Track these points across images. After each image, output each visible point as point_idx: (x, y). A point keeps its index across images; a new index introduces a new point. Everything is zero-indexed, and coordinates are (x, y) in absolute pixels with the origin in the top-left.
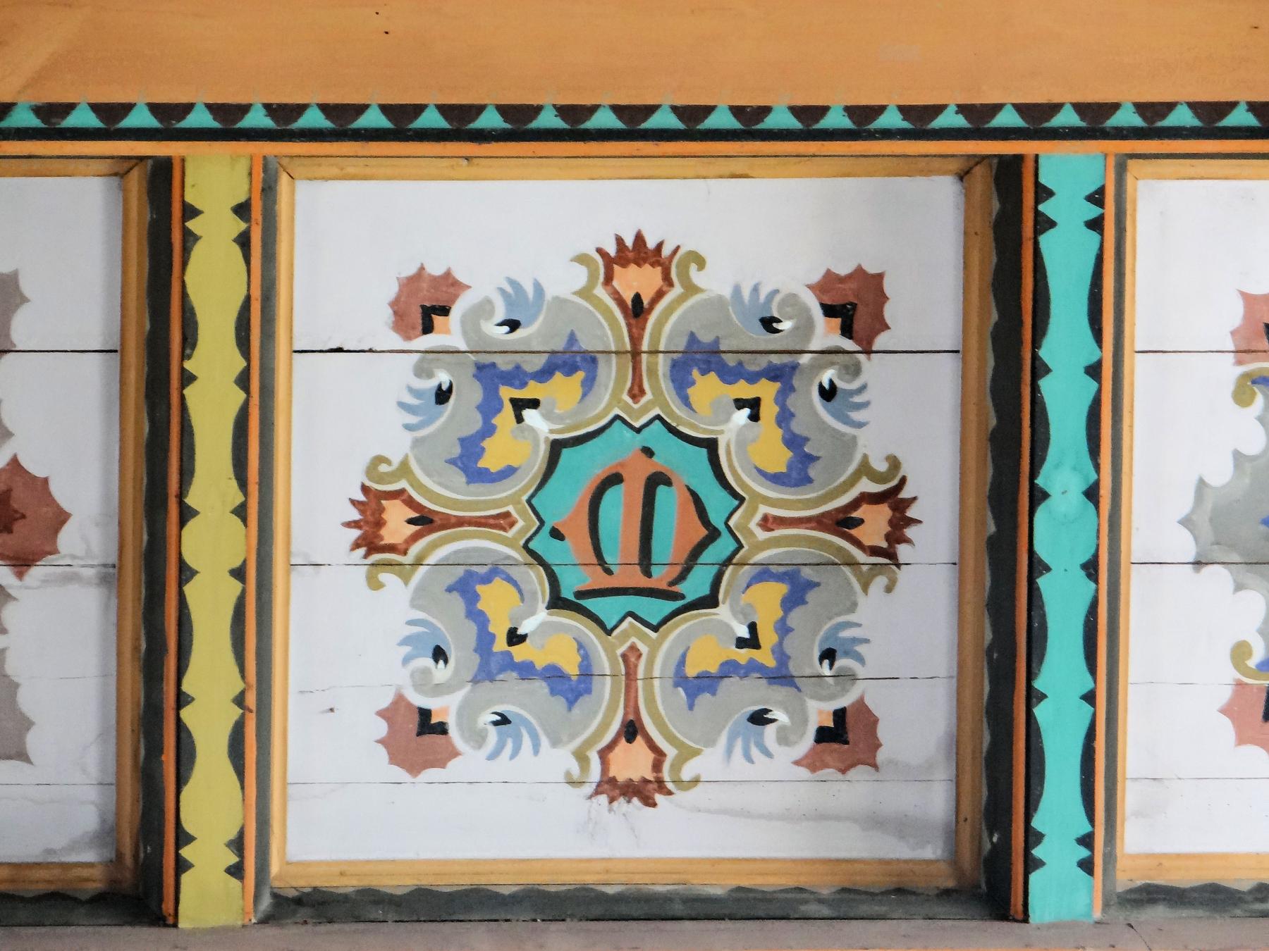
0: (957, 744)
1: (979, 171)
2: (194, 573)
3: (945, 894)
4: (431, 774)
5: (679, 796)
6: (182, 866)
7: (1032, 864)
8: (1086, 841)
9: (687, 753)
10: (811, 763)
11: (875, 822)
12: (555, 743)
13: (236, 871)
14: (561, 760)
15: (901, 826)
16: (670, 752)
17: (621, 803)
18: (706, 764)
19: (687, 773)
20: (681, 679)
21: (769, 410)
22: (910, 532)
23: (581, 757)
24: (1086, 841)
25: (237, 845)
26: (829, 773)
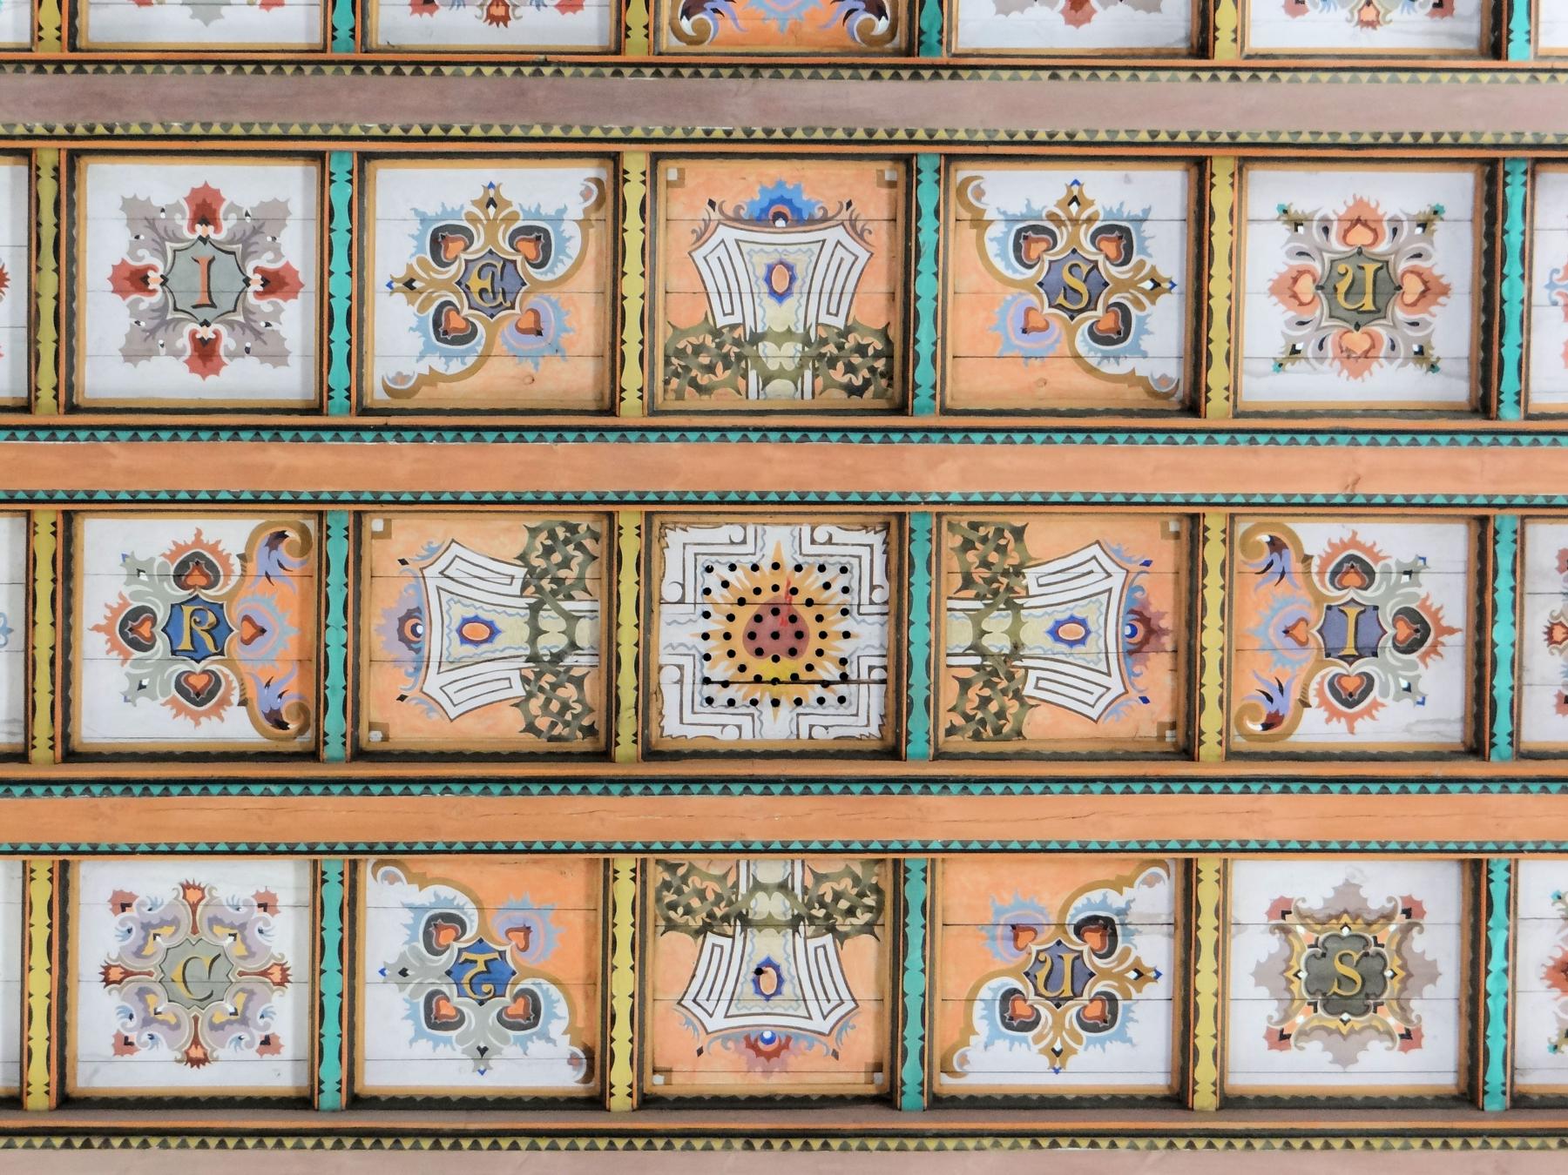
0: (1475, 210)
1: (1300, 1044)
2: (499, 632)
3: (1455, 1098)
4: (1299, 18)
5: (1386, 26)
6: (1216, 39)
7: (1509, 41)
8: (1529, 32)
9: (1388, 11)
10: (1432, 15)
11: (1452, 35)
12: (1343, 7)
13: (1235, 40)
14: (1344, 13)
15: (1463, 37)
16: (1382, 11)
17: (1365, 29)
18: (1395, 15)
19: (1388, 17)
20: (1015, 991)
21: (1137, 639)
22: (1376, 550)
23: (1351, 12)
24: (1529, 32)
25: (1235, 31)
26: (1437, 18)
